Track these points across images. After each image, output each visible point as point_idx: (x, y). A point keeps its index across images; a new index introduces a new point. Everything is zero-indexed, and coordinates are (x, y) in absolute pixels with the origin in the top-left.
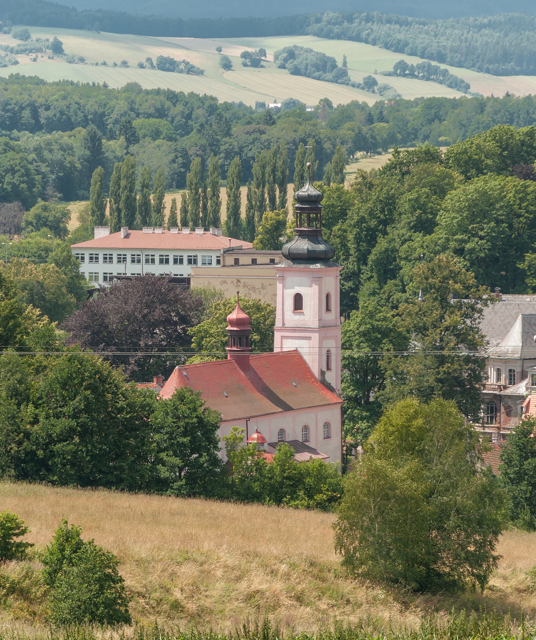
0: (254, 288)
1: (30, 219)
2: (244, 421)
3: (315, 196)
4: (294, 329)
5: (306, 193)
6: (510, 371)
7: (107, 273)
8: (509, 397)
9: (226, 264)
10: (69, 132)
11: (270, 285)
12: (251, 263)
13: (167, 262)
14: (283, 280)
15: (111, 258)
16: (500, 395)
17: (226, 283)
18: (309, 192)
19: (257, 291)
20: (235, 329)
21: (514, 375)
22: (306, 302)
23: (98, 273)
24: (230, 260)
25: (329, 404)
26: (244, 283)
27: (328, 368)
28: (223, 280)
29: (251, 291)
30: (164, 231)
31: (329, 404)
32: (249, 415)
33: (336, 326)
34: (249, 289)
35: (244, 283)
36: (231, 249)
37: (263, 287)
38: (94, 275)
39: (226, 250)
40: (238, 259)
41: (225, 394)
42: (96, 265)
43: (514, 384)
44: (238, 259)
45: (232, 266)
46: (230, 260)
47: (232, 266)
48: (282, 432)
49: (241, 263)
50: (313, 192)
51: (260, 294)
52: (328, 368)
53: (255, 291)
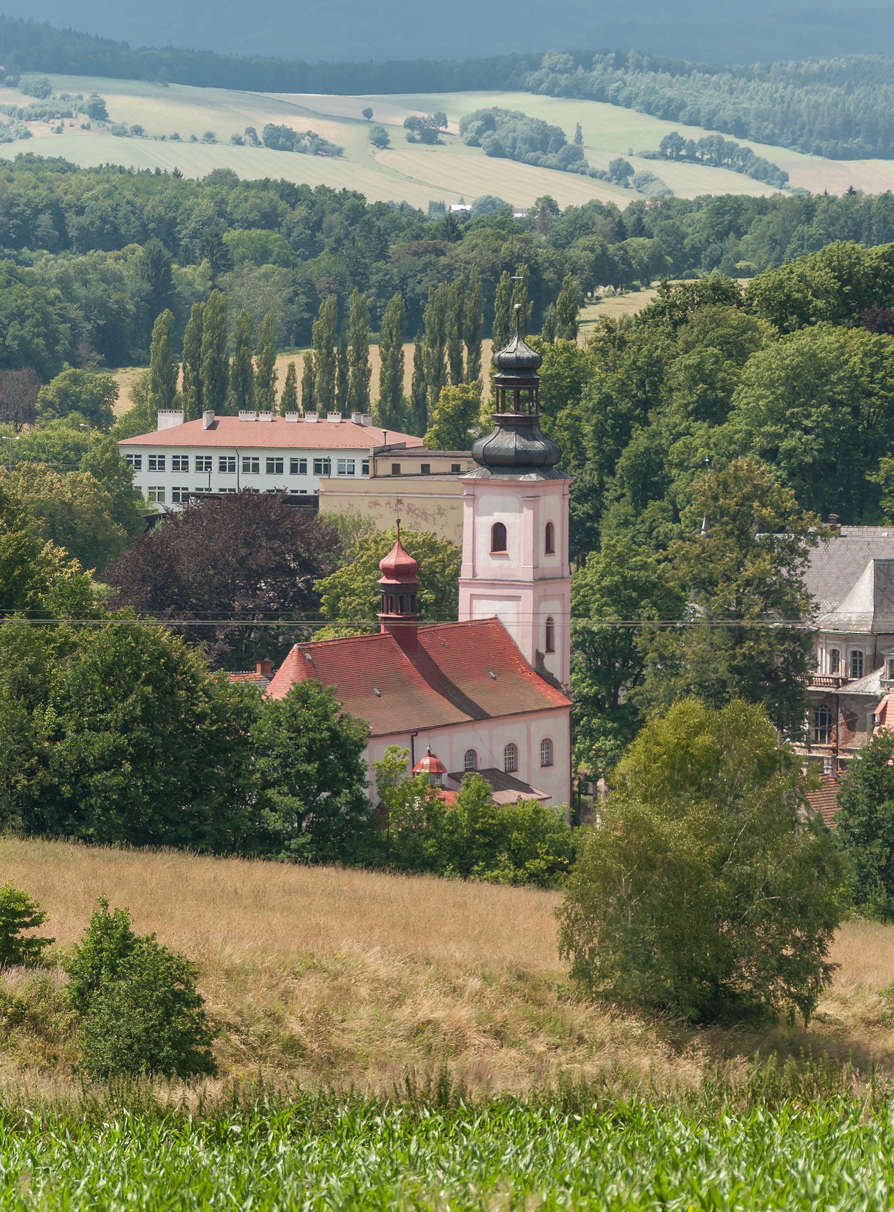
0: (426, 514)
2: (408, 737)
4: (493, 583)
5: (513, 355)
6: (854, 653)
8: (853, 697)
11: (452, 508)
12: (420, 472)
15: (186, 463)
16: (837, 695)
20: (393, 582)
21: (861, 662)
22: (485, 539)
33: (562, 578)
34: (418, 515)
37: (440, 513)
40: (428, 466)
43: (861, 676)
44: (428, 466)
45: (388, 476)
46: (384, 466)
47: (388, 476)
49: (403, 471)
52: (550, 649)
53: (426, 519)
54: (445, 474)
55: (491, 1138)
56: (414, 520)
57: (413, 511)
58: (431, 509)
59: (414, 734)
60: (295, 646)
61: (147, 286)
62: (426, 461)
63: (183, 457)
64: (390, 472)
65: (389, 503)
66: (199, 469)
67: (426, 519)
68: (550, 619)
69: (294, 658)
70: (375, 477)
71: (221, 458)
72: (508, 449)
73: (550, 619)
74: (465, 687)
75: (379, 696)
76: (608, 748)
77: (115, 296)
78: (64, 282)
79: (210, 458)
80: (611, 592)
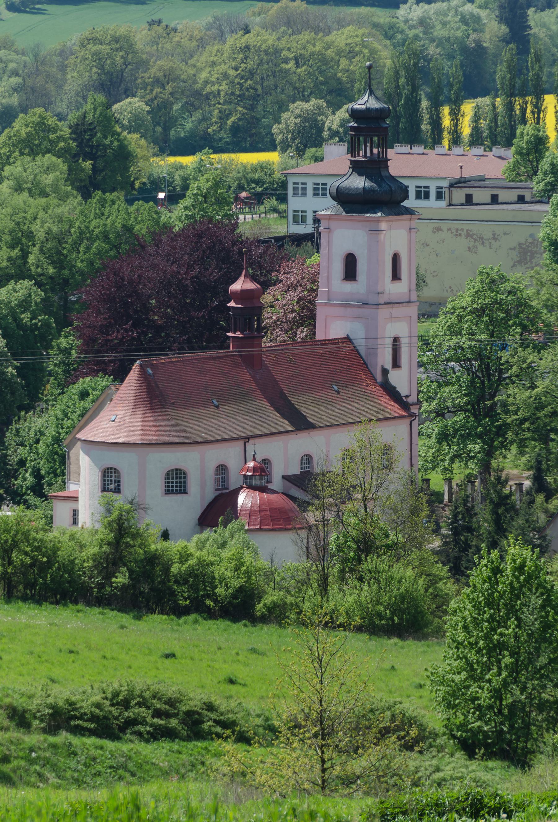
0: (482, 238)
1: (334, 127)
2: (241, 443)
3: (377, 109)
5: (364, 107)
7: (298, 211)
9: (454, 202)
10: (440, 3)
11: (505, 234)
13: (427, 196)
14: (329, 232)
15: (304, 189)
17: (441, 230)
18: (368, 106)
19: (487, 243)
20: (240, 306)
22: (338, 268)
23: (305, 212)
24: (459, 195)
25: (389, 419)
26: (467, 230)
27: (396, 364)
28: (436, 225)
29: (477, 244)
30: (426, 151)
31: (389, 419)
32: (248, 434)
33: (409, 302)
34: (475, 240)
35: (467, 230)
36: (463, 180)
37: (495, 237)
38: (300, 214)
39: (454, 182)
40: (497, 196)
41: (215, 401)
42: (303, 199)
44: (497, 196)
46: (459, 195)
48: (307, 459)
49: (475, 200)
50: (373, 105)
51: (490, 248)
52: (396, 364)
53: (483, 243)
54: (511, 203)
55: (458, 788)
56: (472, 244)
57: (472, 236)
58: (488, 235)
59: (247, 439)
60: (138, 362)
61: (504, 29)
62: (495, 192)
63: (302, 184)
64: (463, 200)
65: (450, 229)
66: (316, 194)
67: (483, 243)
68: (396, 340)
69: (136, 372)
70: (450, 205)
71: (315, 184)
72: (357, 189)
73: (396, 340)
74: (295, 400)
75: (217, 407)
76: (477, 450)
77: (473, 36)
78: (422, 22)
79: (305, 184)
80: (479, 313)
